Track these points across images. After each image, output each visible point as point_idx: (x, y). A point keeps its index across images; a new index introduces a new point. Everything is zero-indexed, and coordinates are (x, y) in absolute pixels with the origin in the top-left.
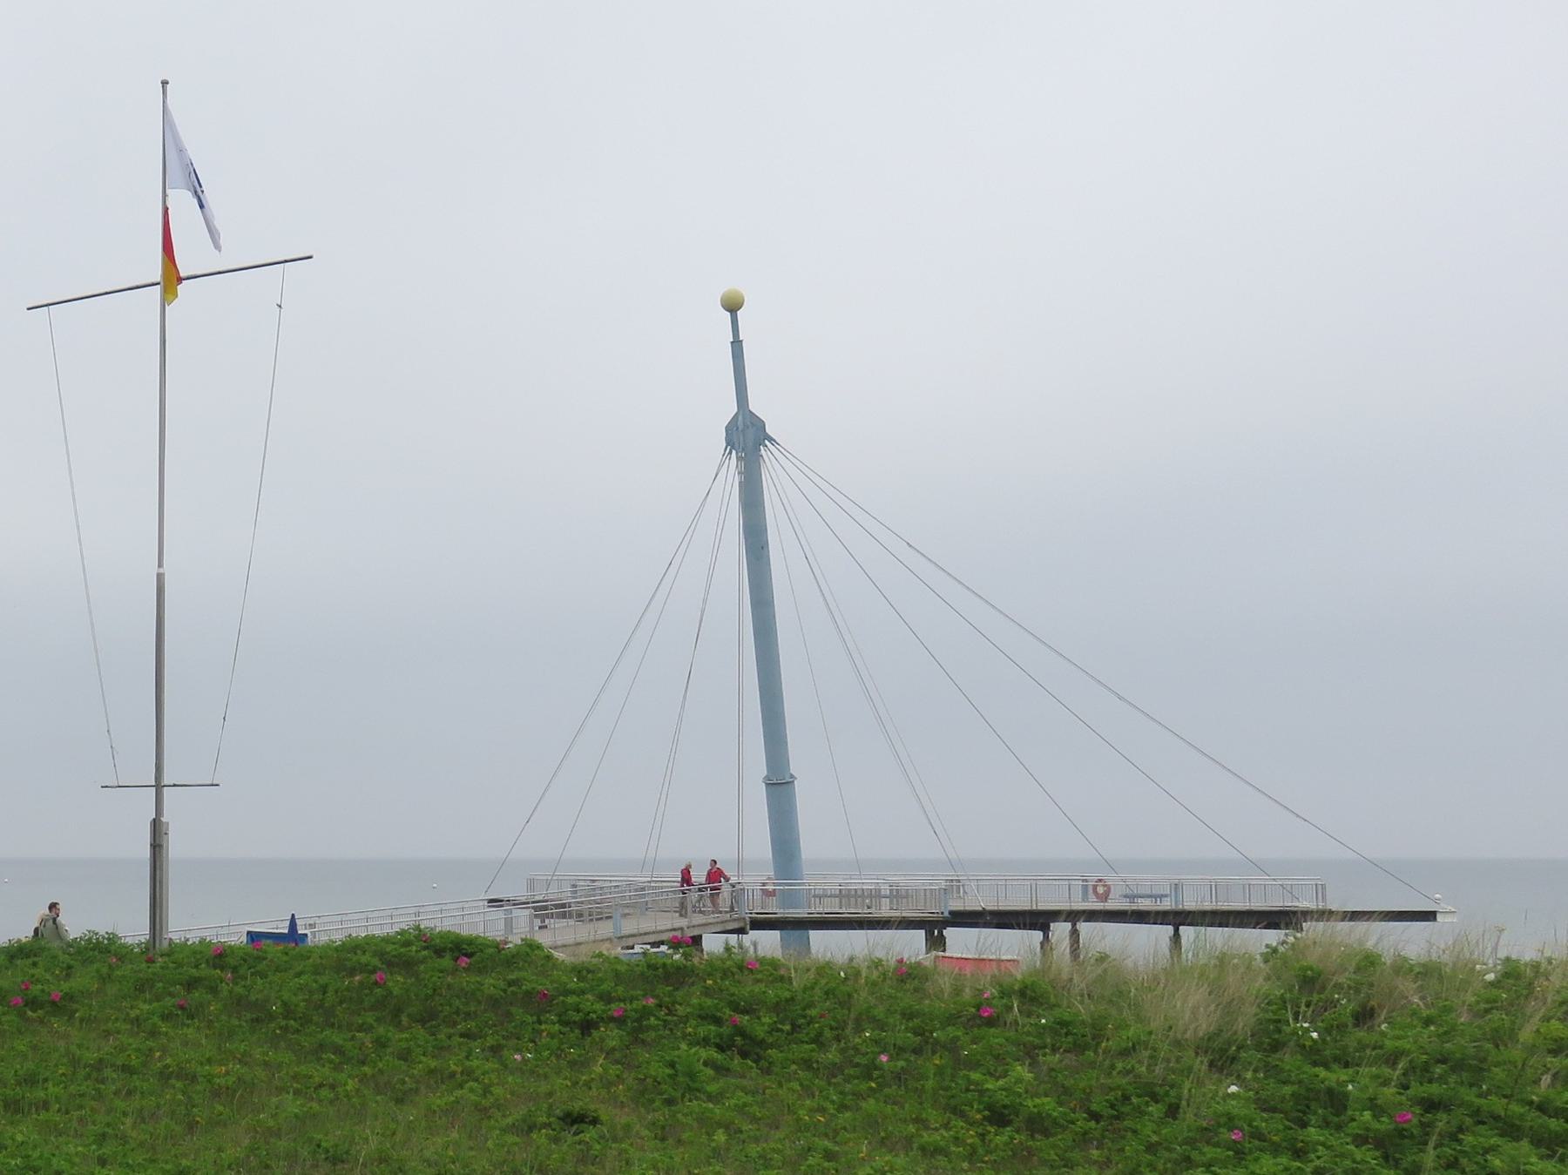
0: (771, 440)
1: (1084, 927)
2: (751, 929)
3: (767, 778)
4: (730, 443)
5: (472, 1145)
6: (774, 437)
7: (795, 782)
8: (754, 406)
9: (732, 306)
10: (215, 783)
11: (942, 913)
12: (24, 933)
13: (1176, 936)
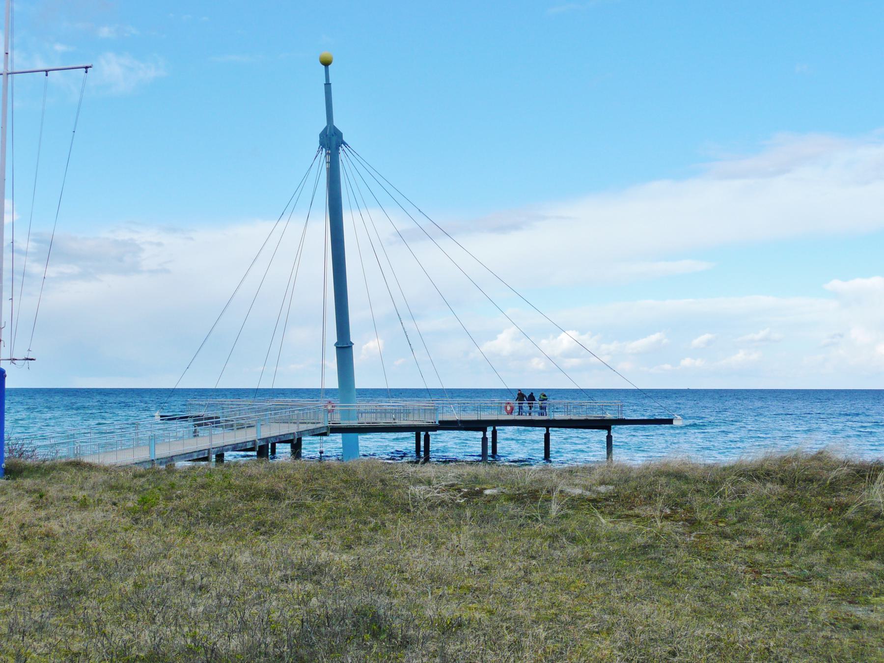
0: (344, 143)
1: (556, 435)
2: (330, 433)
3: (336, 344)
4: (323, 144)
5: (122, 512)
6: (346, 142)
7: (353, 346)
8: (338, 123)
9: (326, 64)
10: (30, 357)
11: (435, 422)
12: (345, 139)
13: (547, 436)
